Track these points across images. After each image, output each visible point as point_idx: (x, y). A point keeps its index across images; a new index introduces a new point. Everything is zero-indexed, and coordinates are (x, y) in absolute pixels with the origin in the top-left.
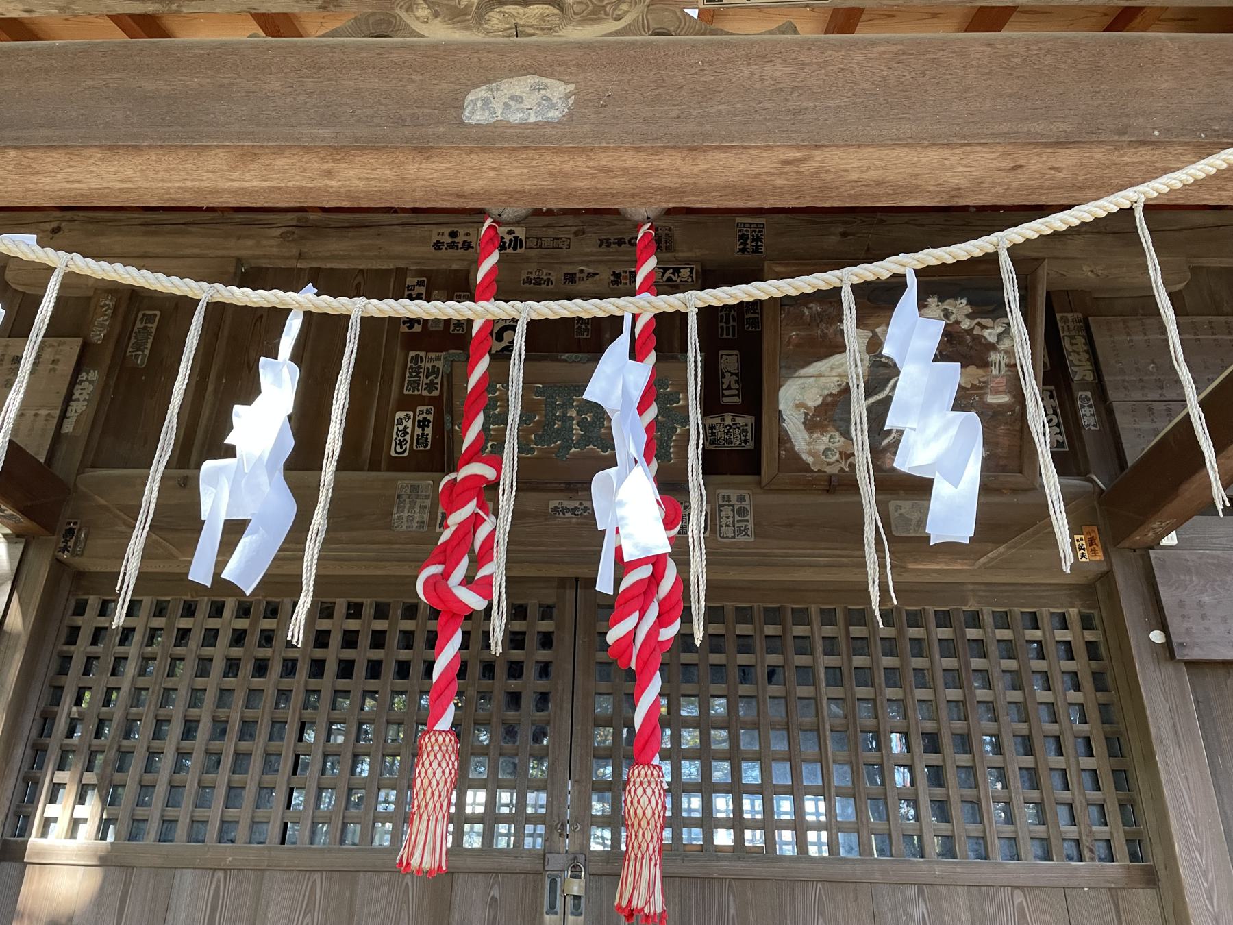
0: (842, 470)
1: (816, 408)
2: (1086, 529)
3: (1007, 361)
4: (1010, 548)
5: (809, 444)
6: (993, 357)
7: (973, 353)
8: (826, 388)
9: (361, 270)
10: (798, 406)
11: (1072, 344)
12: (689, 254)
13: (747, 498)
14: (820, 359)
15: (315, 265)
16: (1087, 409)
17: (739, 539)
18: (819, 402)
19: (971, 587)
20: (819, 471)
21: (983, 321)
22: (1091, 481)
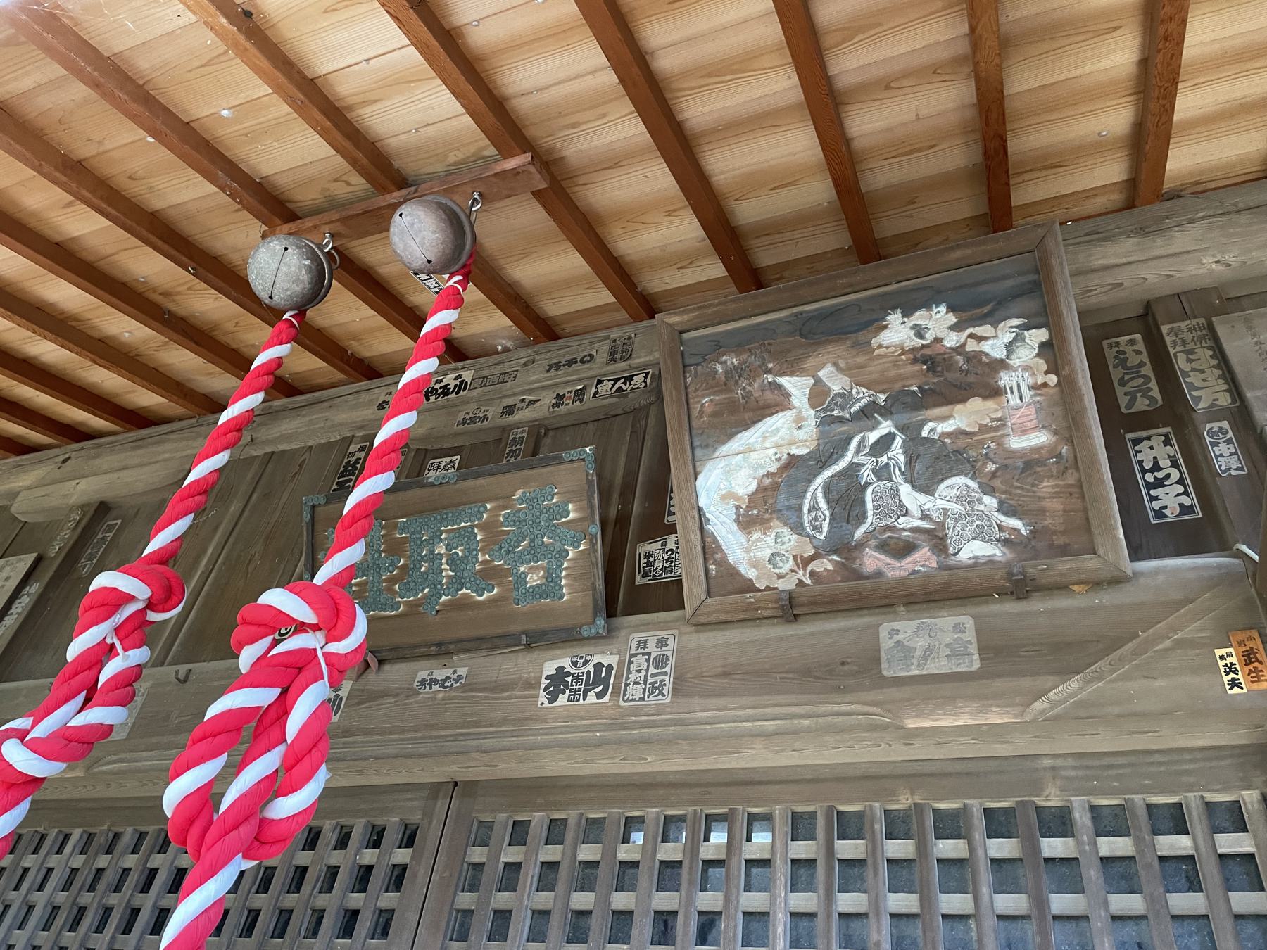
0: (801, 583)
1: (751, 497)
2: (1234, 638)
3: (1030, 381)
4: (1089, 682)
5: (747, 550)
6: (1005, 379)
7: (971, 379)
8: (761, 466)
9: (311, 447)
10: (724, 498)
11: (1189, 361)
12: (647, 359)
13: (670, 642)
14: (746, 426)
15: (268, 449)
16: (1223, 446)
17: (651, 700)
18: (753, 487)
19: (1047, 762)
20: (768, 588)
21: (978, 330)
22: (1240, 555)
